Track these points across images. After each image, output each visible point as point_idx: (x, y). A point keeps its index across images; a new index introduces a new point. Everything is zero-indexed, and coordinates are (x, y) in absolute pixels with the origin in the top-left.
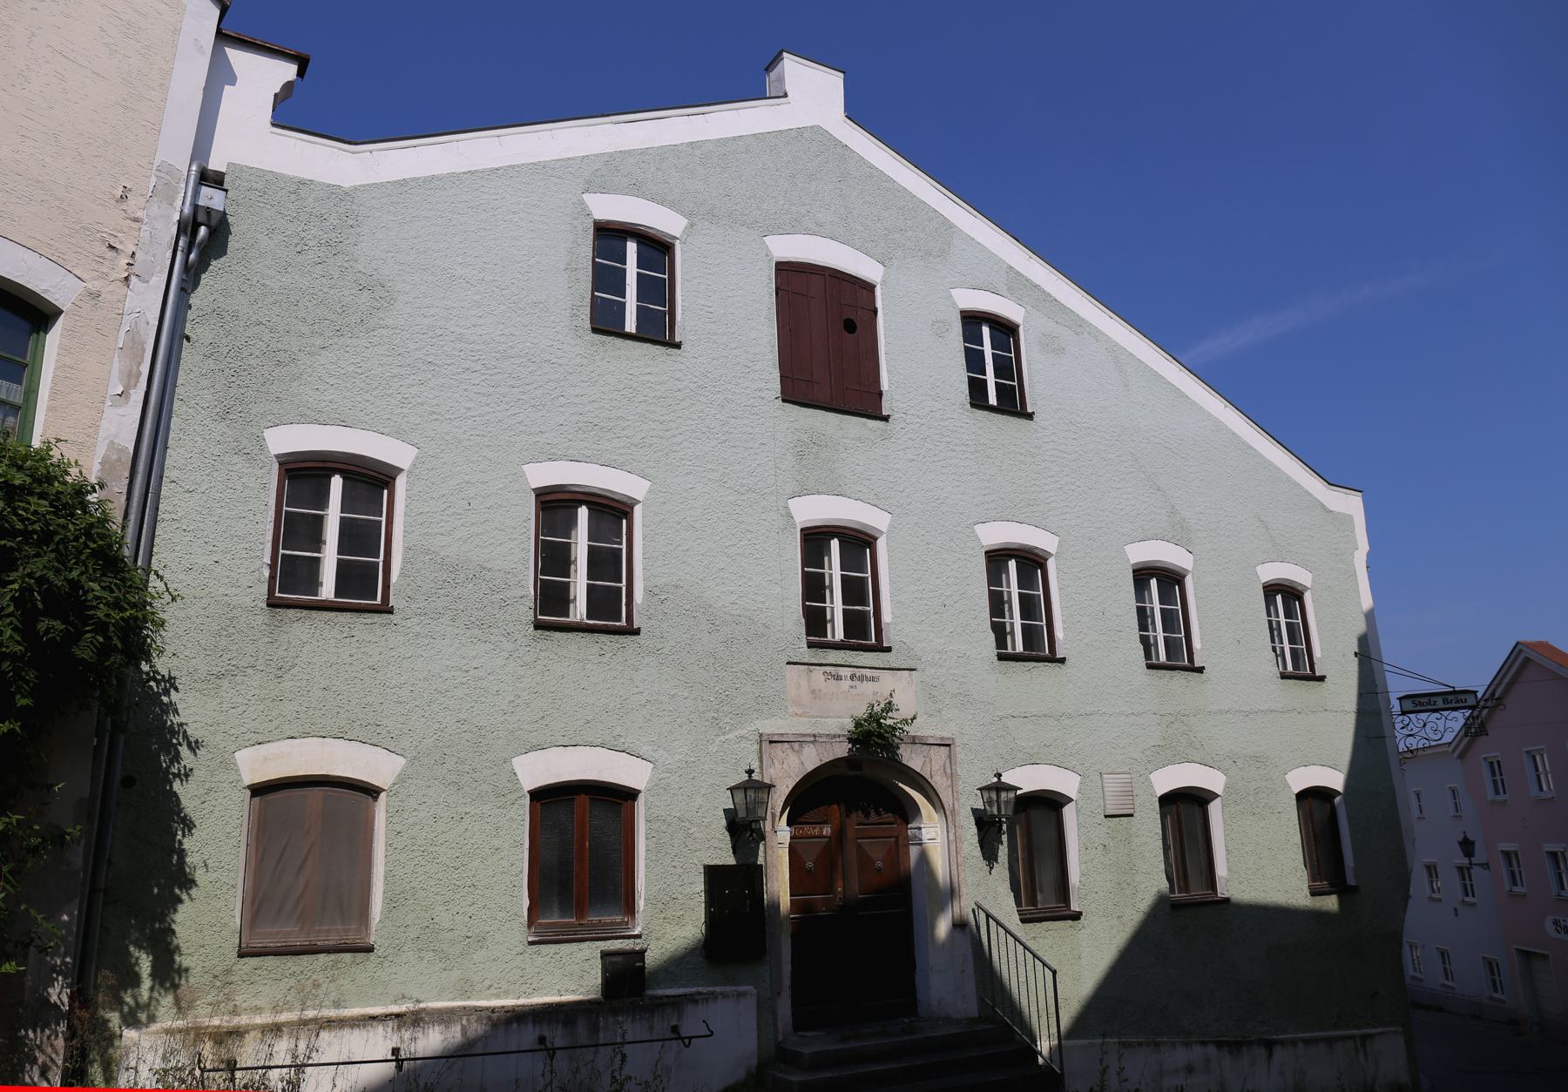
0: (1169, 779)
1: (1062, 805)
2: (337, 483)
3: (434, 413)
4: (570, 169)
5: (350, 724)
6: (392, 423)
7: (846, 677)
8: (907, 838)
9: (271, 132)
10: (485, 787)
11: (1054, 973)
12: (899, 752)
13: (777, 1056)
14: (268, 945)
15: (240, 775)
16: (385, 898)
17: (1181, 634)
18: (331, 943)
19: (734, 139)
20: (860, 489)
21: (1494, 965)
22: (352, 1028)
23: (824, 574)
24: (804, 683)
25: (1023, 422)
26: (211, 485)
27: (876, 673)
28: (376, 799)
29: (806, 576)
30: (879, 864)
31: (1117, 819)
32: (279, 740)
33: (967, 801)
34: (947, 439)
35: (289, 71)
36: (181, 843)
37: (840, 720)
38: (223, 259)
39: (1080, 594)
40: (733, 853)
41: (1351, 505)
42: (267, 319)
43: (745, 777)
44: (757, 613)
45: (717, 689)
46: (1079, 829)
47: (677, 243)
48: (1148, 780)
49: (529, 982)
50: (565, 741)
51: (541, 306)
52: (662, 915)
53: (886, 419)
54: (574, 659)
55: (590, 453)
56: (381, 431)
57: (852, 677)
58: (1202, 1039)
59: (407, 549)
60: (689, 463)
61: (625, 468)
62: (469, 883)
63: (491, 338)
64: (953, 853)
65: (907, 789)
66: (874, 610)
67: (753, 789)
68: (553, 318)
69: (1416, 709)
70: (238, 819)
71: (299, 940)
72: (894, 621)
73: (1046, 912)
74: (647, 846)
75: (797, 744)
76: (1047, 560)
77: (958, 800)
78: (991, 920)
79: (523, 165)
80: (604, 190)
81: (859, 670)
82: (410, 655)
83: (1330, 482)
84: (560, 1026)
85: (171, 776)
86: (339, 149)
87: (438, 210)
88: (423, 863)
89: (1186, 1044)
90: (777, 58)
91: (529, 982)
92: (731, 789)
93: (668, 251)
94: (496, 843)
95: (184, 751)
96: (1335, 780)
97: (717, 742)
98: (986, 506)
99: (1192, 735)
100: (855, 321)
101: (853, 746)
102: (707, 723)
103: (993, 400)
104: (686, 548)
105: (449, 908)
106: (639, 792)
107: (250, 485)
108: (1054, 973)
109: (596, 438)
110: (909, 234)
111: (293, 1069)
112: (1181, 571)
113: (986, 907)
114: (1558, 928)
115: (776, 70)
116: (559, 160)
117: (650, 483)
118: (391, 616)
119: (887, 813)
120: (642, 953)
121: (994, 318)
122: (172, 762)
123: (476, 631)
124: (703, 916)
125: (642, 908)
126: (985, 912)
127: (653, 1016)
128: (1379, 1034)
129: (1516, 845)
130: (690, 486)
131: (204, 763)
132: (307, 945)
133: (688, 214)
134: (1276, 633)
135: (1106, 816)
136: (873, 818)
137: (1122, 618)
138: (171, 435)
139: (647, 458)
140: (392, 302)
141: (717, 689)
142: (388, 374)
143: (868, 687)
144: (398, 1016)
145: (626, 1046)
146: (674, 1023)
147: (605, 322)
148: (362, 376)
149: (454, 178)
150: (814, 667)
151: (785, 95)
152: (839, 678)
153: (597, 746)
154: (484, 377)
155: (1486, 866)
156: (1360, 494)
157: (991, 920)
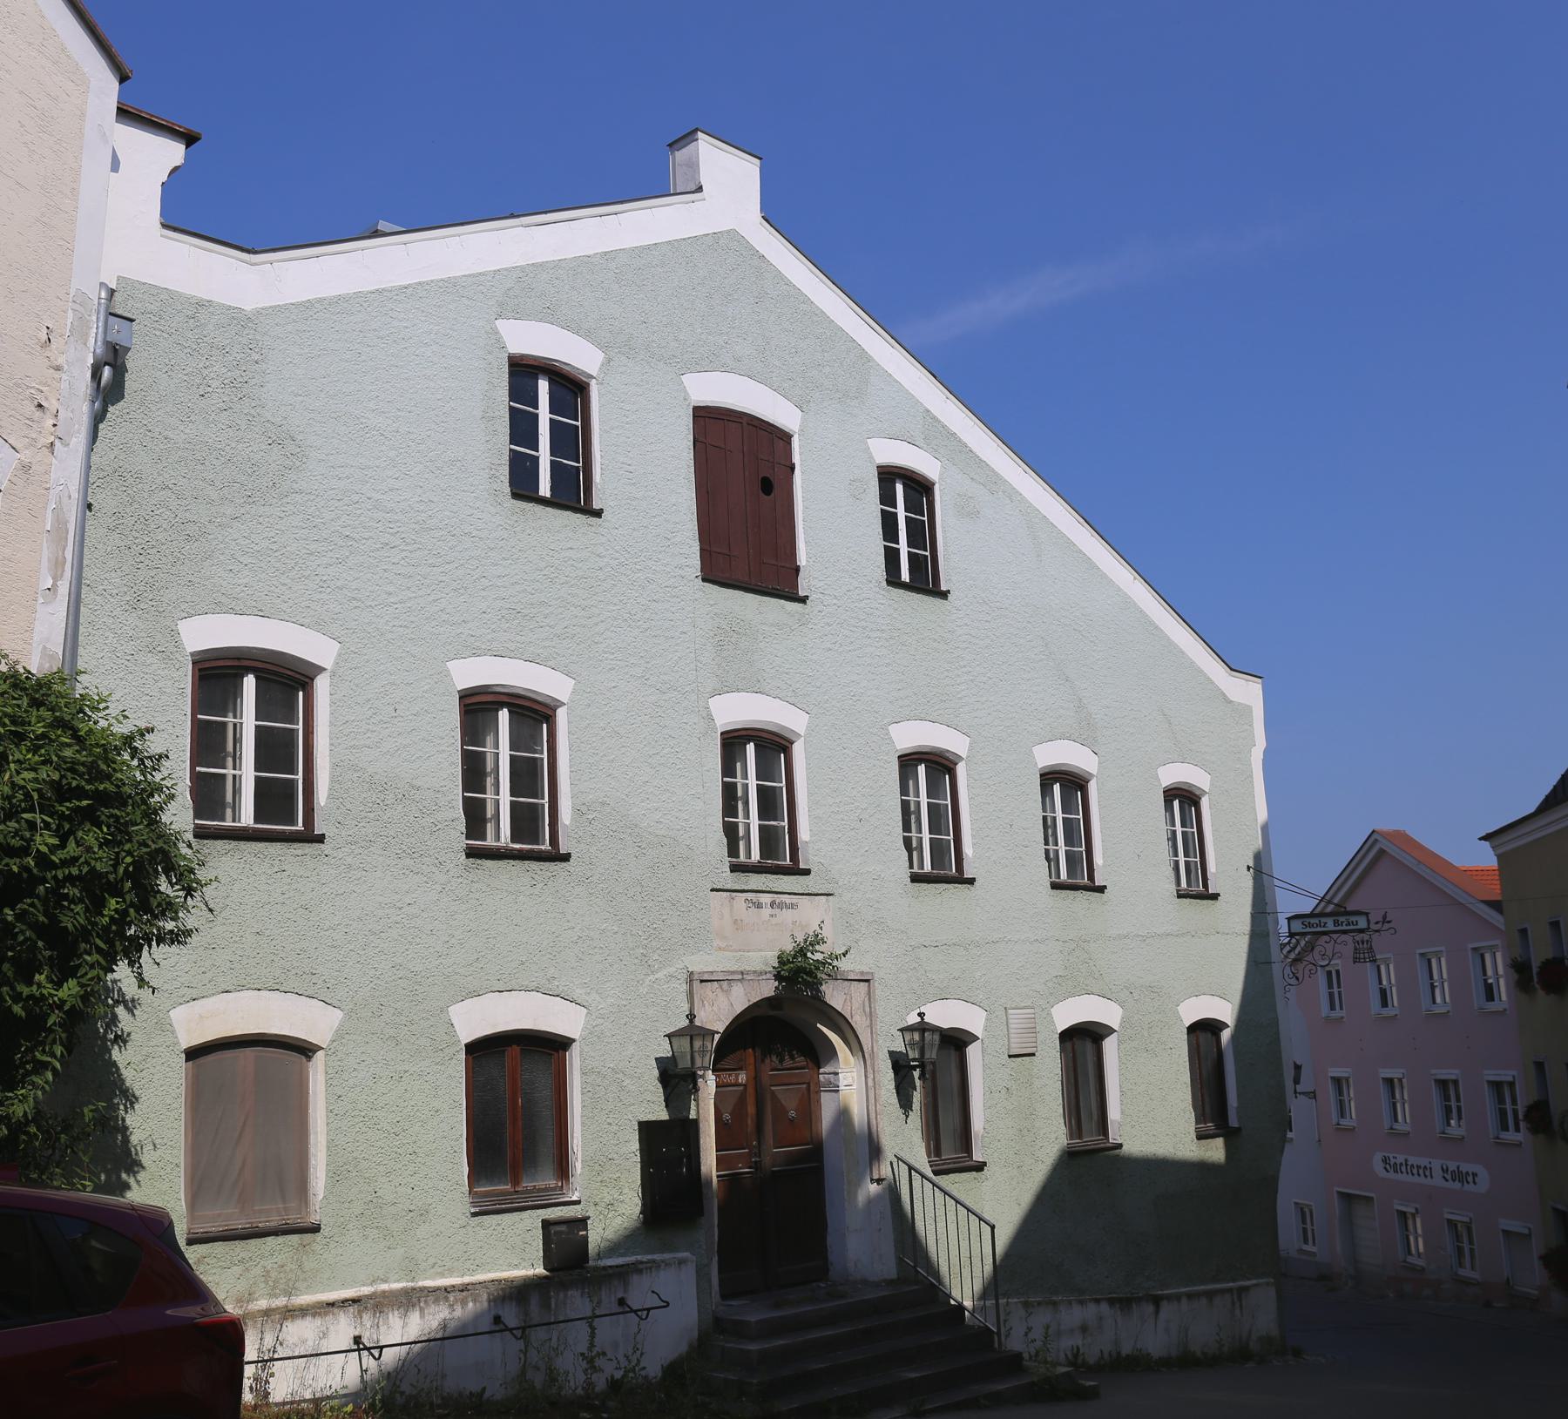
0: (1068, 1014)
1: (966, 1044)
2: (249, 682)
3: (355, 599)
4: (481, 287)
5: (285, 973)
6: (312, 613)
7: (766, 904)
9: (162, 236)
11: (993, 1227)
12: (823, 988)
13: (715, 1328)
14: (210, 1230)
15: (176, 1037)
16: (328, 1171)
17: (1081, 847)
18: (272, 1224)
19: (648, 247)
20: (779, 685)
21: (1306, 1210)
22: (314, 1317)
23: (735, 784)
25: (938, 601)
26: (126, 691)
28: (309, 1058)
29: (725, 785)
30: (792, 1113)
31: (1020, 1059)
32: (213, 994)
33: (886, 1040)
34: (864, 623)
35: (173, 152)
36: (124, 1120)
37: (763, 954)
38: (122, 403)
39: (989, 804)
40: (666, 1106)
41: (1248, 693)
42: (173, 481)
44: (682, 832)
45: (645, 921)
46: (984, 1071)
47: (593, 383)
48: (1050, 1014)
49: (472, 1257)
51: (459, 464)
52: (599, 1178)
53: (803, 600)
54: (506, 891)
55: (512, 646)
56: (300, 622)
57: (772, 905)
58: (1094, 1297)
59: (335, 766)
60: (612, 657)
61: (549, 663)
62: (411, 1151)
63: (409, 505)
64: (872, 1101)
65: (824, 1029)
66: (304, 779)
67: (692, 1031)
69: (1304, 931)
70: (178, 1088)
71: (240, 1224)
72: (813, 839)
73: (949, 1163)
74: (583, 1101)
76: (956, 764)
77: (877, 1041)
78: (913, 1173)
79: (432, 281)
80: (518, 315)
81: (779, 896)
82: (342, 891)
84: (514, 1304)
85: (109, 1043)
86: (237, 259)
88: (364, 1130)
89: (1081, 1302)
90: (689, 137)
91: (472, 1257)
92: (669, 1036)
93: (581, 392)
95: (120, 1011)
96: (1225, 1011)
97: (647, 982)
99: (1092, 964)
100: (772, 479)
101: (780, 983)
102: (636, 961)
103: (545, 489)
104: (611, 758)
105: (390, 1179)
106: (574, 1040)
108: (993, 1227)
109: (520, 628)
110: (827, 369)
111: (260, 1364)
112: (1086, 776)
113: (905, 1157)
114: (1388, 1167)
115: (684, 150)
116: (470, 275)
117: (574, 682)
118: (322, 846)
119: (801, 1056)
120: (582, 1222)
121: (920, 479)
122: (108, 1026)
123: (408, 861)
124: (639, 1177)
125: (579, 1171)
126: (907, 1165)
127: (600, 1289)
129: (1349, 1070)
130: (613, 685)
131: (140, 1025)
132: (249, 1228)
133: (603, 347)
134: (1050, 831)
135: (1010, 1056)
136: (788, 1063)
137: (1028, 831)
138: (82, 629)
140: (304, 460)
141: (645, 921)
142: (305, 551)
143: (787, 915)
144: (355, 1301)
145: (596, 1320)
146: (620, 1295)
147: (522, 483)
150: (735, 894)
151: (700, 189)
152: (759, 906)
153: (533, 990)
154: (404, 554)
155: (1312, 1095)
156: (1260, 680)
157: (913, 1173)
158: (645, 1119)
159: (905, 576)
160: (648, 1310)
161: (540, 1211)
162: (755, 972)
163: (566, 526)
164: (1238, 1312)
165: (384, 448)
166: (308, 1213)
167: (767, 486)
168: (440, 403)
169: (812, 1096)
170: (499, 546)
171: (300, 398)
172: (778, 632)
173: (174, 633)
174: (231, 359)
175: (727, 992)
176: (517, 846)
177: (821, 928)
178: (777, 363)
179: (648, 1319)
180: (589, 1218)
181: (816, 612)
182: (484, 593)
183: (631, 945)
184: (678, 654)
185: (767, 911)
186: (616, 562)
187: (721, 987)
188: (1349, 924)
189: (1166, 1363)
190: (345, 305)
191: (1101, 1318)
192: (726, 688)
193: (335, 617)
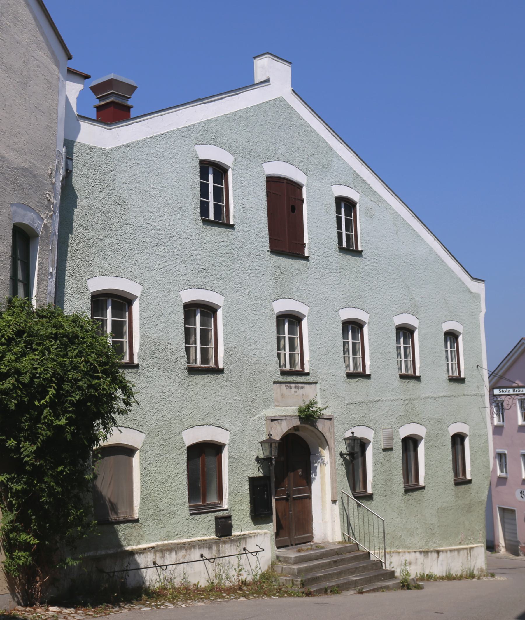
0: (405, 431)
6: (133, 274)
10: (173, 446)
19: (248, 108)
24: (279, 390)
27: (303, 385)
34: (329, 267)
42: (84, 223)
43: (268, 437)
44: (263, 358)
48: (398, 431)
50: (200, 423)
53: (307, 259)
57: (295, 387)
66: (129, 341)
68: (187, 215)
75: (280, 421)
79: (172, 131)
83: (473, 277)
84: (207, 549)
87: (142, 159)
92: (261, 443)
94: (178, 471)
98: (343, 300)
102: (247, 412)
107: (84, 308)
109: (205, 276)
110: (316, 156)
112: (362, 323)
116: (185, 127)
128: (476, 547)
139: (222, 285)
143: (301, 391)
144: (153, 548)
146: (244, 547)
148: (120, 250)
149: (147, 142)
153: (211, 425)
154: (164, 248)
158: (251, 476)
159: (211, 217)
160: (167, 566)
161: (214, 514)
162: (290, 416)
163: (221, 232)
164: (469, 558)
165: (156, 204)
166: (133, 514)
167: (293, 209)
168: (176, 183)
170: (197, 242)
171: (127, 185)
172: (297, 272)
173: (86, 285)
174: (103, 170)
175: (280, 424)
176: (203, 366)
177: (316, 398)
178: (298, 155)
179: (167, 570)
180: (232, 516)
181: (312, 263)
182: (192, 262)
183: (245, 406)
184: (261, 284)
185: (293, 390)
186: (239, 246)
187: (278, 423)
188: (519, 391)
189: (442, 578)
190: (142, 144)
191: (417, 559)
192: (278, 298)
193: (141, 275)
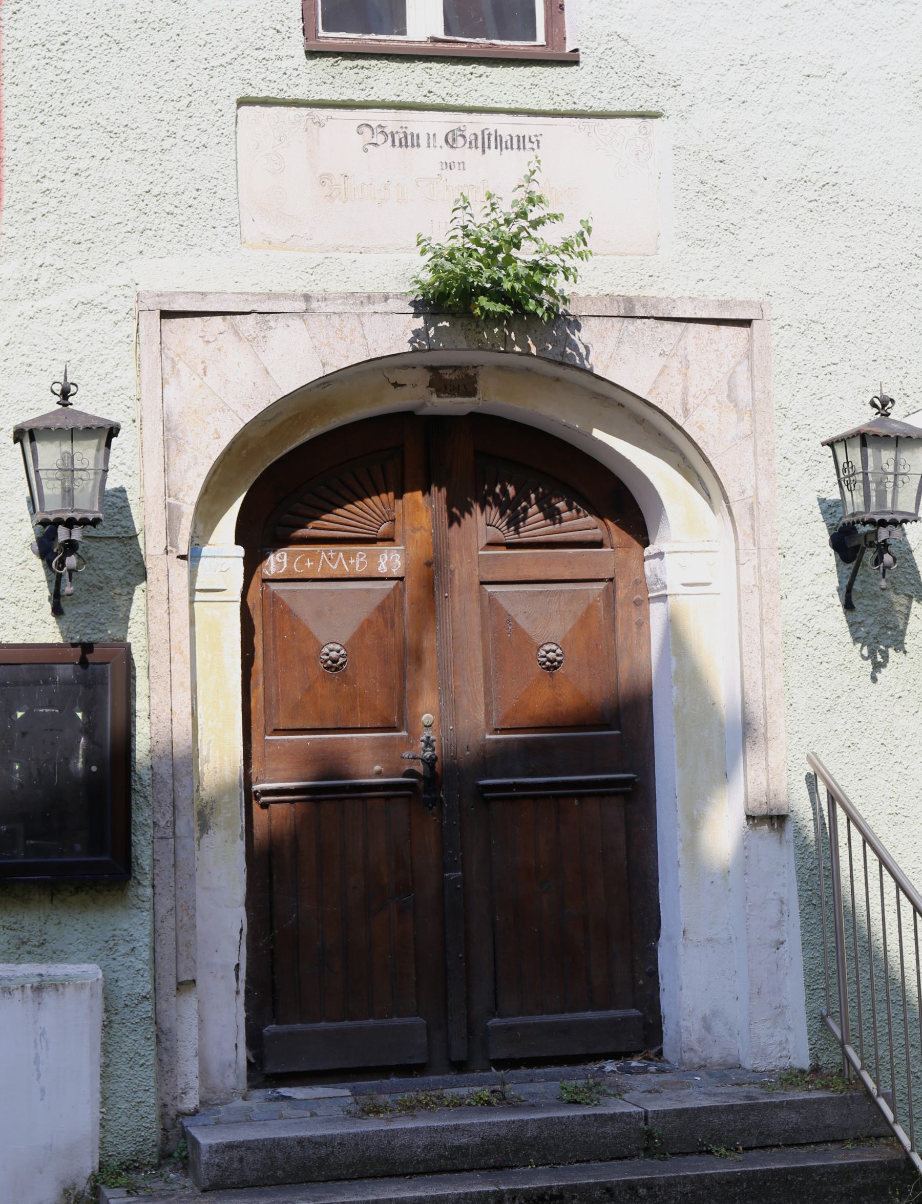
8: (641, 583)
43: (51, 404)
57: (450, 141)
81: (474, 117)
169: (621, 613)
